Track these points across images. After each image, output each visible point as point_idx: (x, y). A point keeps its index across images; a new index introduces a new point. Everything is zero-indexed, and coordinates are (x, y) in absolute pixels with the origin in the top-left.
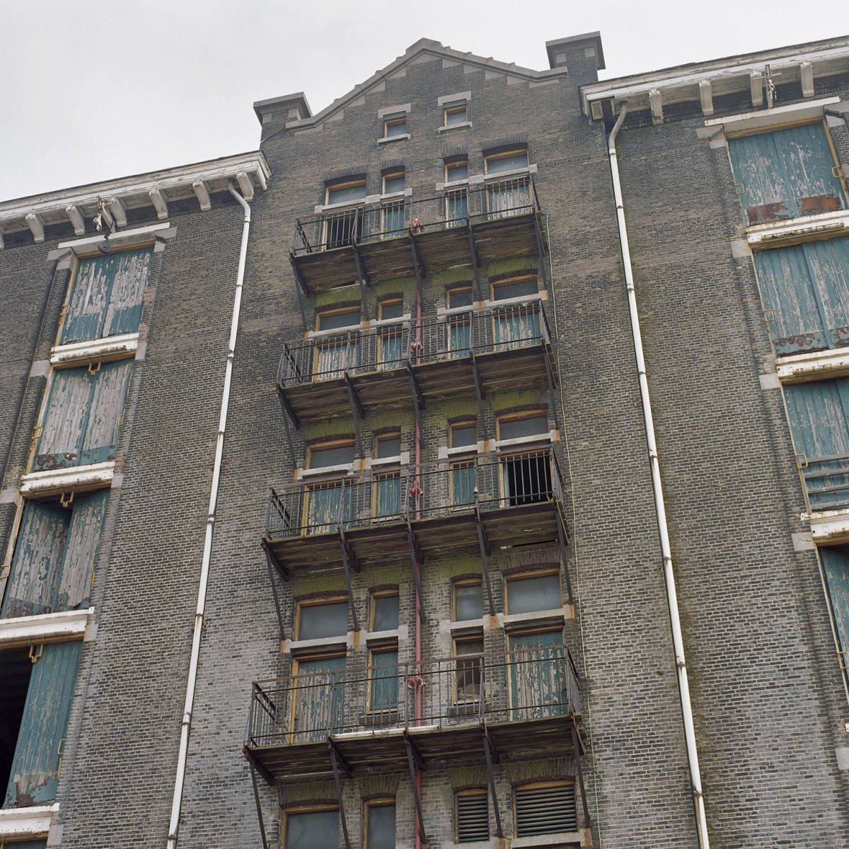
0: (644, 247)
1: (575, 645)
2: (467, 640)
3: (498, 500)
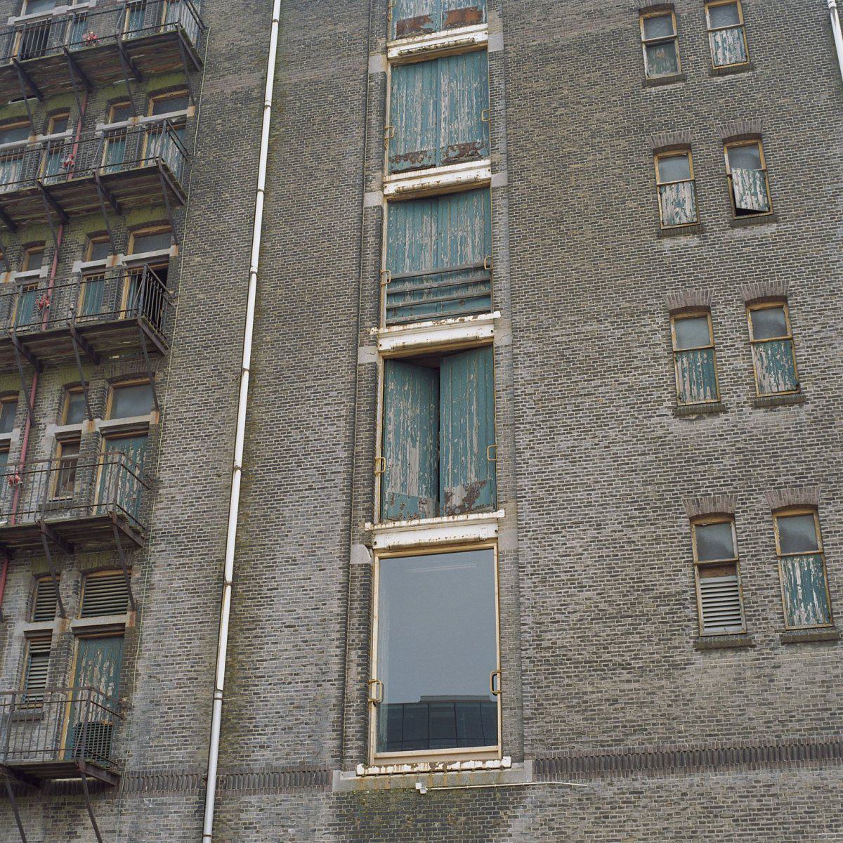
0: (289, 62)
1: (153, 448)
2: (69, 442)
3: (117, 312)
